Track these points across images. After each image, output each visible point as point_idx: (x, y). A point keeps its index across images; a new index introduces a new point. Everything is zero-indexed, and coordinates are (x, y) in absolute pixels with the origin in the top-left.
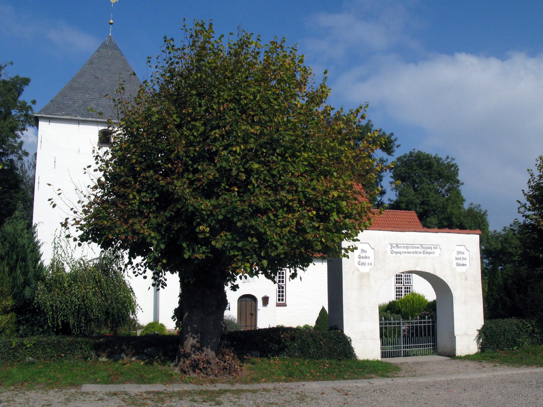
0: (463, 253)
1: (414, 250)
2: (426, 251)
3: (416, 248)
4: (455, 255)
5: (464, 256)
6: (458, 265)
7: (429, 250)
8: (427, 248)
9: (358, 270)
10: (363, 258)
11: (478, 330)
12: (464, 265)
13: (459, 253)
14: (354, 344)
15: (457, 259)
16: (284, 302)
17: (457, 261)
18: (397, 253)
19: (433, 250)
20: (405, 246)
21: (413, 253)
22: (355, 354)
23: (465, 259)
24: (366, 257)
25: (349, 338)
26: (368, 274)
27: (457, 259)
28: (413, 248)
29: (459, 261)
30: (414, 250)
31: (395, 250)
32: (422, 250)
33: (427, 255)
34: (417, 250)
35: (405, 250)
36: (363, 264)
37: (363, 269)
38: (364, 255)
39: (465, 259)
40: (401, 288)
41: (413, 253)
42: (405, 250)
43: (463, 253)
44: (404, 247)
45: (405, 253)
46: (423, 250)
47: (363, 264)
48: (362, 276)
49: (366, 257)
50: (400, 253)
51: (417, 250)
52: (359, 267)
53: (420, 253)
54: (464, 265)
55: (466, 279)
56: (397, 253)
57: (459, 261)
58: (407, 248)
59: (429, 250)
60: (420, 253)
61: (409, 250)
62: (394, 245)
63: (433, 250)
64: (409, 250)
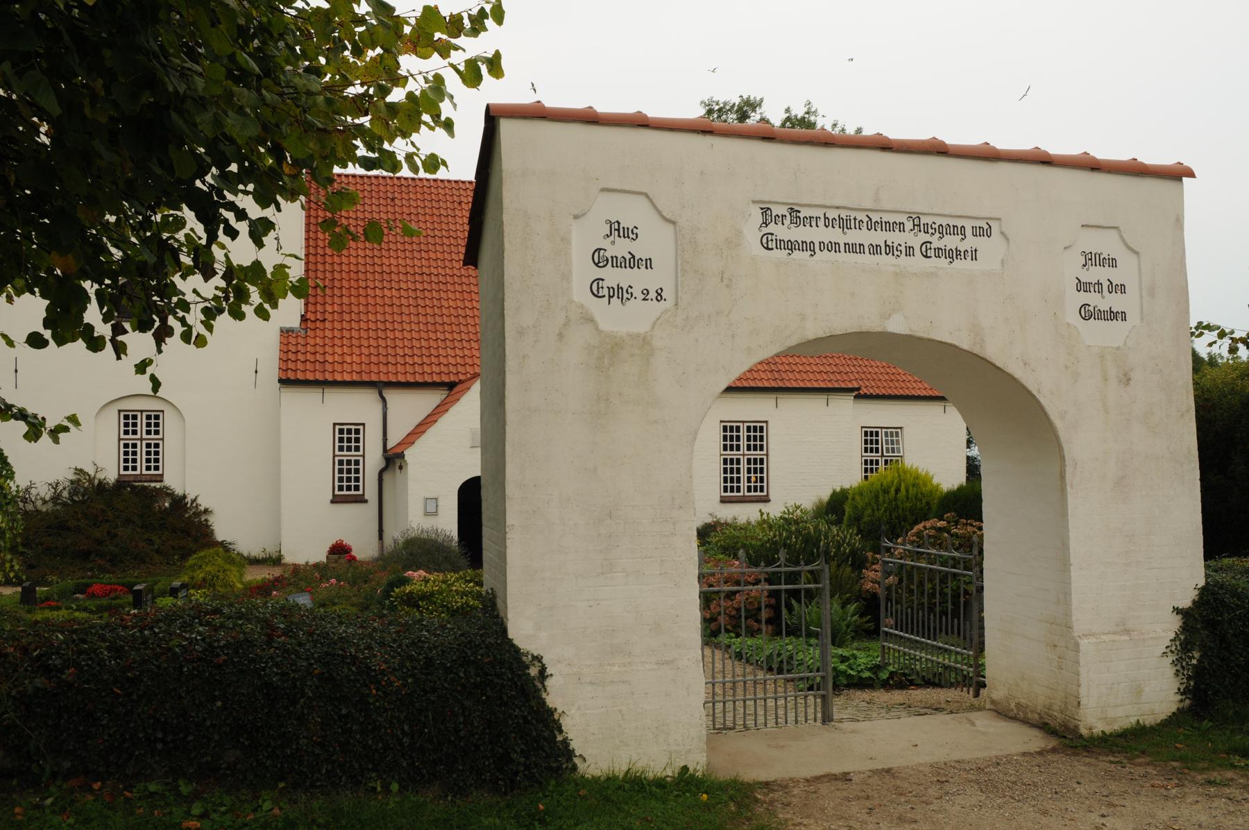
0: (1113, 263)
1: (878, 237)
2: (936, 243)
3: (889, 226)
4: (1073, 268)
5: (1116, 276)
6: (1087, 313)
7: (951, 242)
8: (943, 231)
9: (590, 320)
10: (616, 262)
11: (1177, 611)
12: (1113, 315)
13: (1092, 259)
14: (556, 695)
15: (1082, 286)
16: (360, 492)
17: (1084, 298)
18: (791, 246)
19: (971, 242)
20: (832, 214)
21: (875, 250)
22: (566, 742)
23: (1122, 288)
24: (632, 262)
25: (538, 659)
26: (644, 342)
27: (1082, 286)
28: (872, 225)
29: (1093, 299)
30: (878, 237)
31: (782, 231)
32: (916, 240)
33: (943, 262)
34: (895, 238)
35: (835, 235)
36: (619, 293)
37: (614, 319)
38: (621, 248)
39: (1122, 288)
40: (134, 446)
41: (875, 250)
42: (835, 235)
43: (1113, 263)
44: (828, 223)
45: (833, 247)
46: (924, 237)
47: (619, 293)
48: (610, 351)
49: (632, 262)
50: (809, 247)
51: (895, 238)
52: (597, 307)
53: (909, 251)
54: (1113, 315)
55: (1126, 380)
56: (791, 246)
57: (1093, 299)
58: (844, 224)
59: (951, 242)
60: (909, 251)
61: (854, 236)
62: (777, 210)
63: (971, 242)
64: (854, 236)
